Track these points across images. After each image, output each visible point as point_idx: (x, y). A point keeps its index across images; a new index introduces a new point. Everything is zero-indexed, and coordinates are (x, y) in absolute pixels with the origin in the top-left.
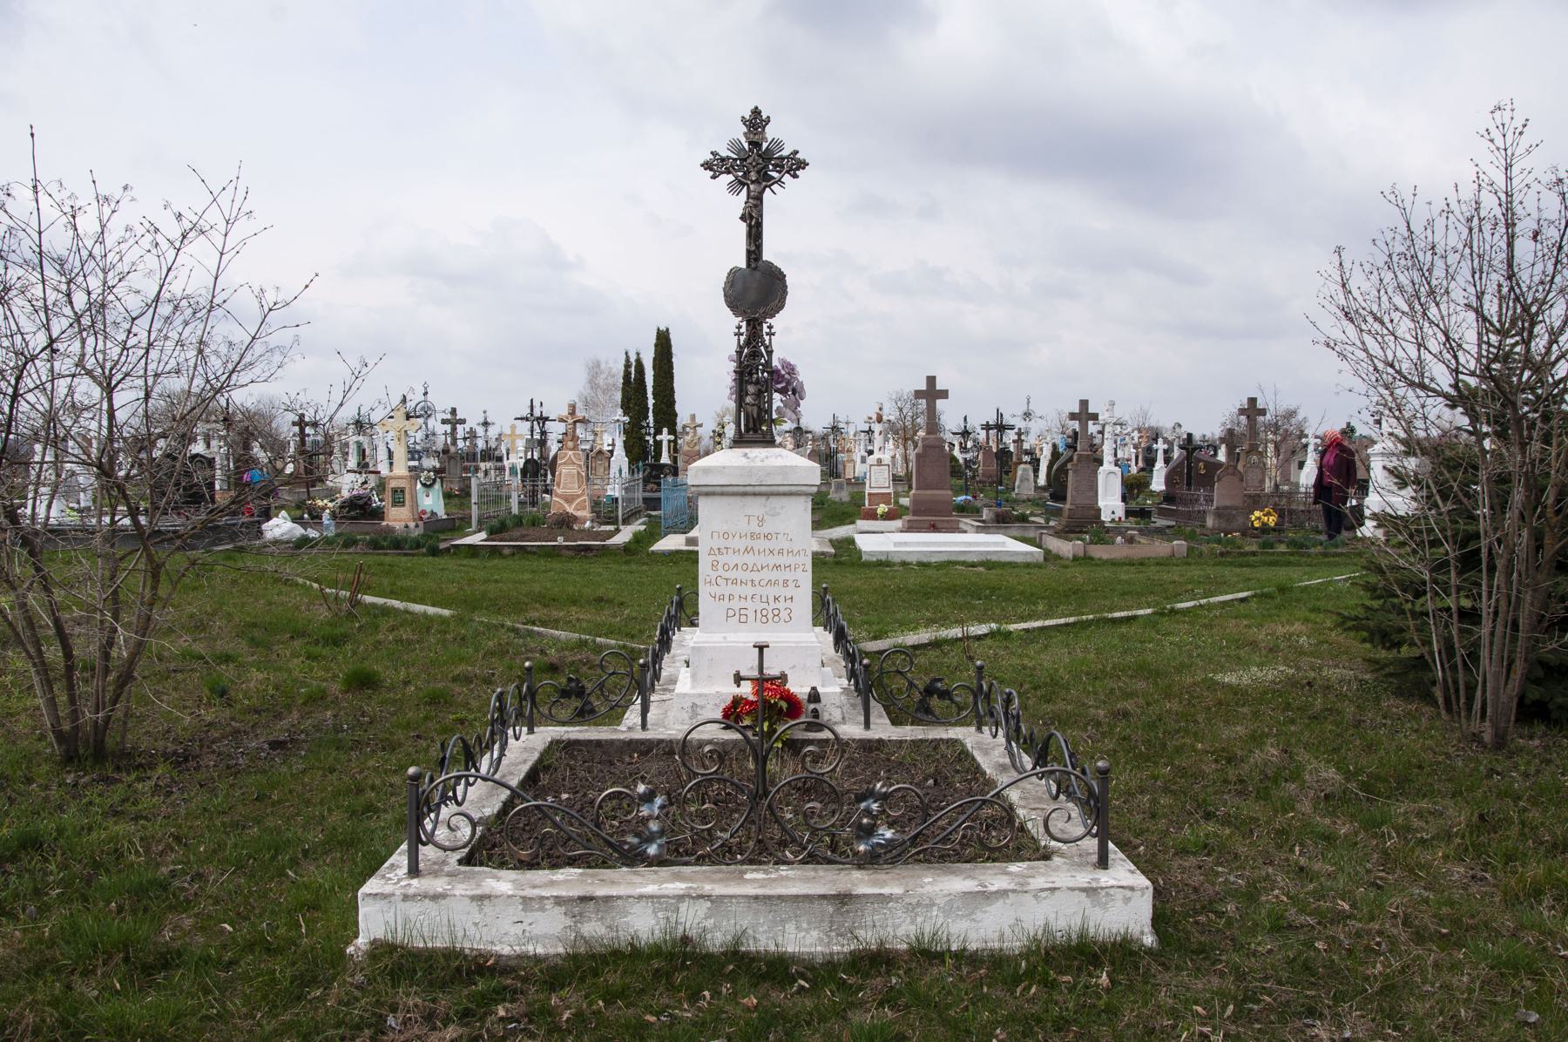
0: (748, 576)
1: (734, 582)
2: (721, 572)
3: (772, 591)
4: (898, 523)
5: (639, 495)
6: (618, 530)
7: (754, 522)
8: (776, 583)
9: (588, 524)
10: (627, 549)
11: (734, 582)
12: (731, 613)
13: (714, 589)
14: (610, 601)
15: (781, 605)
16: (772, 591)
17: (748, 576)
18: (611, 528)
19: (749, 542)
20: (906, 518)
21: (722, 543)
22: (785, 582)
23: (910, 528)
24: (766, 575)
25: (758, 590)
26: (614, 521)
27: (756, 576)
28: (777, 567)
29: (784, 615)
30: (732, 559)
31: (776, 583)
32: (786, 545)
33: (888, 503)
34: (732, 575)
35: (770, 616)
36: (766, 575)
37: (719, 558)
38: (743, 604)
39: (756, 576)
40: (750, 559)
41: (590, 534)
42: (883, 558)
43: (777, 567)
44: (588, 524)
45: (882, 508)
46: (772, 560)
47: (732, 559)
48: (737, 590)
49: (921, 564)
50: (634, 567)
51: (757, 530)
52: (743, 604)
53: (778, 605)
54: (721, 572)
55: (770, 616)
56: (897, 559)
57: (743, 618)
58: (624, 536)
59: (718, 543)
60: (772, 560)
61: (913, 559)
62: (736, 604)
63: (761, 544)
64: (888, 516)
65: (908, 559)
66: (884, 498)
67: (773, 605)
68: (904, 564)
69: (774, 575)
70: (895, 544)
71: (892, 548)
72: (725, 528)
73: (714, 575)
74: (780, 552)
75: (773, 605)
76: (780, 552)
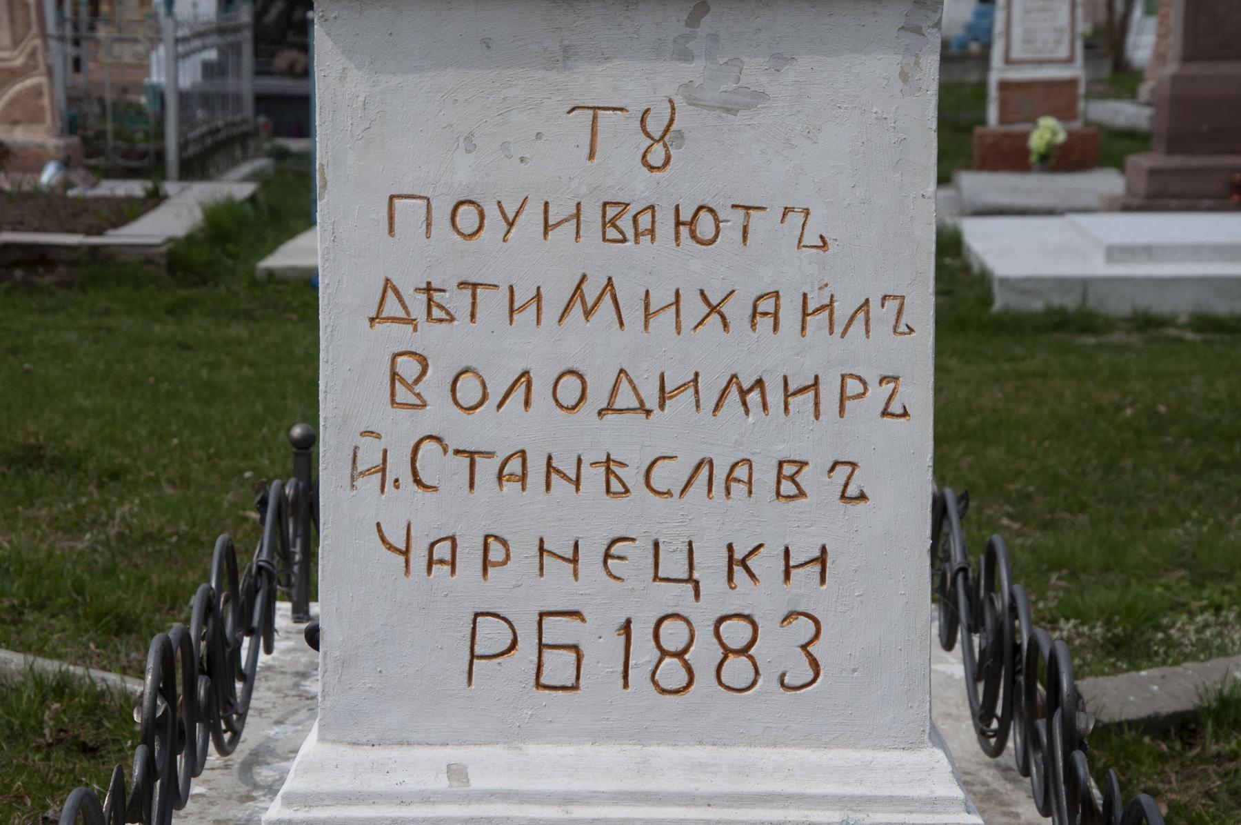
0: (588, 436)
1: (513, 470)
2: (439, 414)
3: (713, 523)
4: (1108, 182)
5: (245, 83)
6: (155, 199)
7: (623, 144)
8: (738, 476)
9: (49, 175)
10: (179, 263)
11: (513, 470)
12: (492, 635)
13: (403, 508)
14: (70, 465)
15: (764, 596)
16: (713, 523)
17: (588, 436)
18: (136, 188)
19: (595, 256)
20: (1143, 161)
21: (445, 259)
22: (789, 472)
23: (1157, 197)
24: (680, 433)
25: (641, 515)
26: (148, 165)
27: (630, 441)
28: (745, 390)
29: (778, 648)
30: (499, 346)
31: (738, 476)
32: (793, 274)
33: (1065, 113)
34: (498, 430)
35: (704, 653)
36: (680, 433)
37: (429, 337)
38: (558, 588)
39: (630, 441)
40: (596, 346)
41: (55, 209)
42: (1070, 302)
43: (745, 390)
44: (49, 175)
45: (1046, 132)
46: (716, 354)
47: (499, 346)
48: (529, 513)
49: (1206, 324)
50: (197, 326)
51: (639, 187)
52: (558, 588)
53: (744, 596)
54: (439, 414)
55: (704, 653)
56: (1118, 306)
57: (559, 666)
58: (177, 215)
59: (418, 257)
60: (716, 354)
61: (1181, 305)
62: (520, 590)
63: (659, 265)
64: (1062, 159)
65: (1161, 305)
66: (1056, 96)
67: (718, 595)
68: (1146, 323)
69: (730, 435)
70: (1114, 253)
71: (1098, 267)
72: (463, 174)
73: (400, 430)
74: (766, 308)
75: (718, 595)
76: (766, 308)
